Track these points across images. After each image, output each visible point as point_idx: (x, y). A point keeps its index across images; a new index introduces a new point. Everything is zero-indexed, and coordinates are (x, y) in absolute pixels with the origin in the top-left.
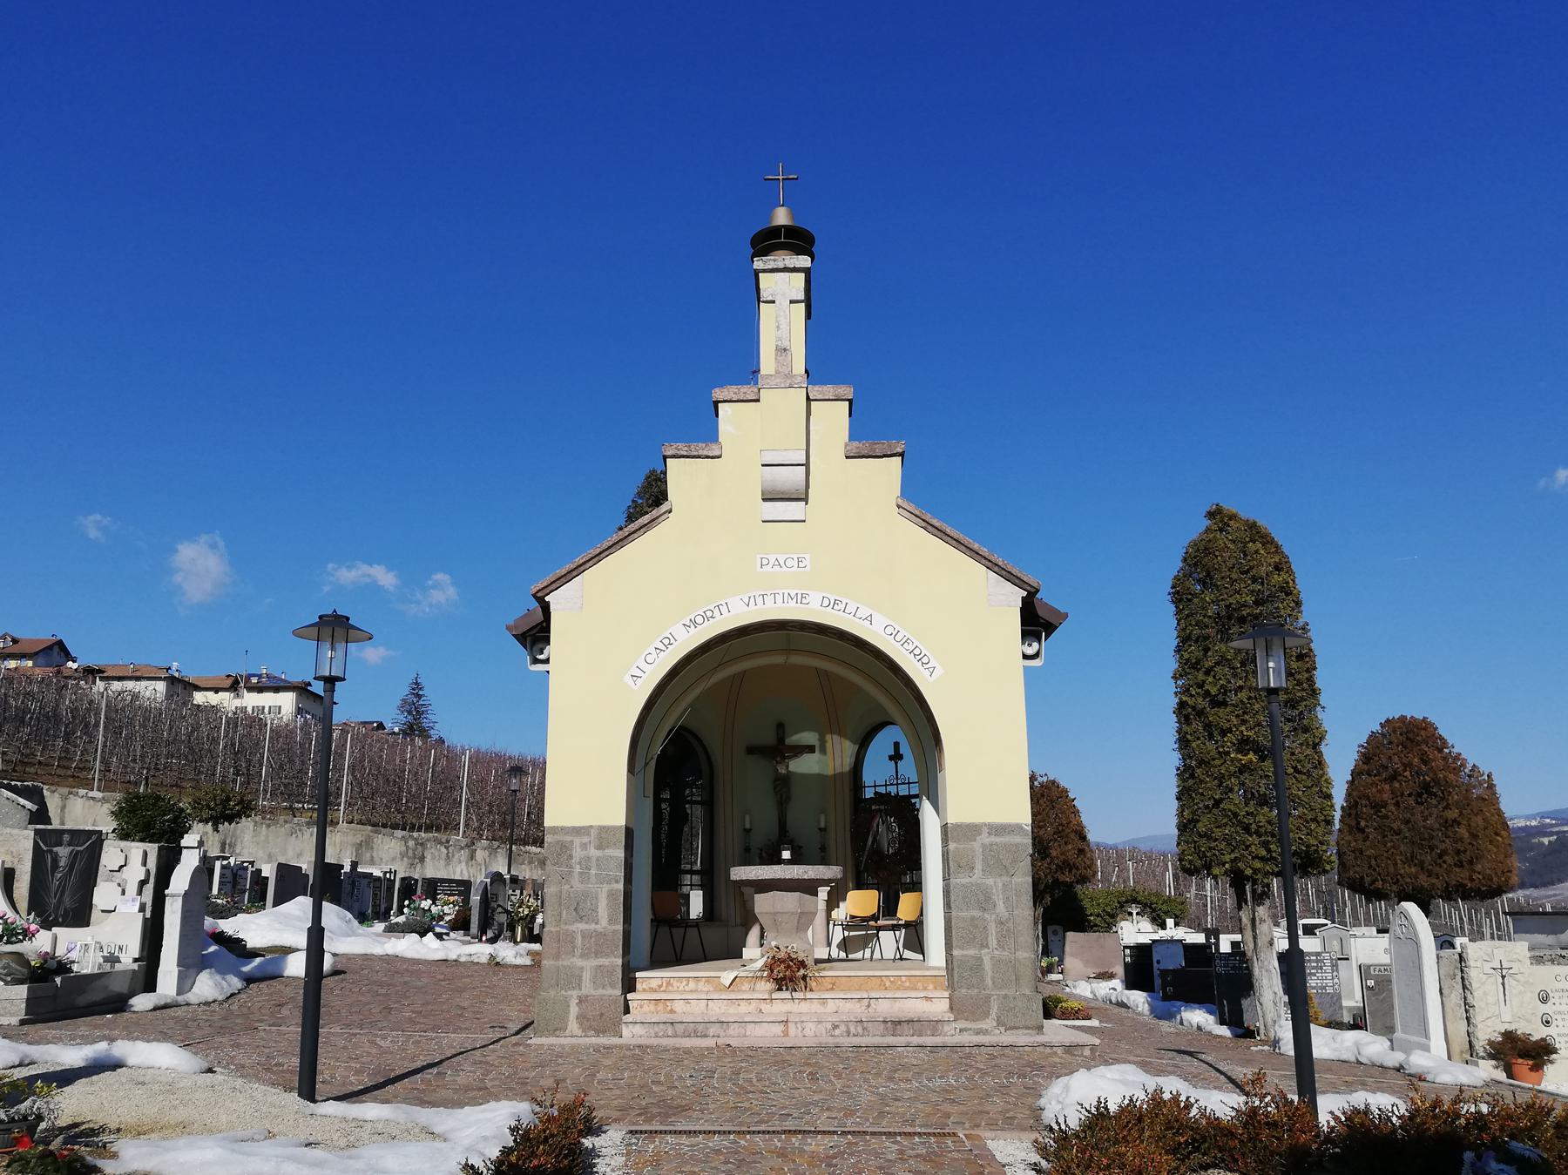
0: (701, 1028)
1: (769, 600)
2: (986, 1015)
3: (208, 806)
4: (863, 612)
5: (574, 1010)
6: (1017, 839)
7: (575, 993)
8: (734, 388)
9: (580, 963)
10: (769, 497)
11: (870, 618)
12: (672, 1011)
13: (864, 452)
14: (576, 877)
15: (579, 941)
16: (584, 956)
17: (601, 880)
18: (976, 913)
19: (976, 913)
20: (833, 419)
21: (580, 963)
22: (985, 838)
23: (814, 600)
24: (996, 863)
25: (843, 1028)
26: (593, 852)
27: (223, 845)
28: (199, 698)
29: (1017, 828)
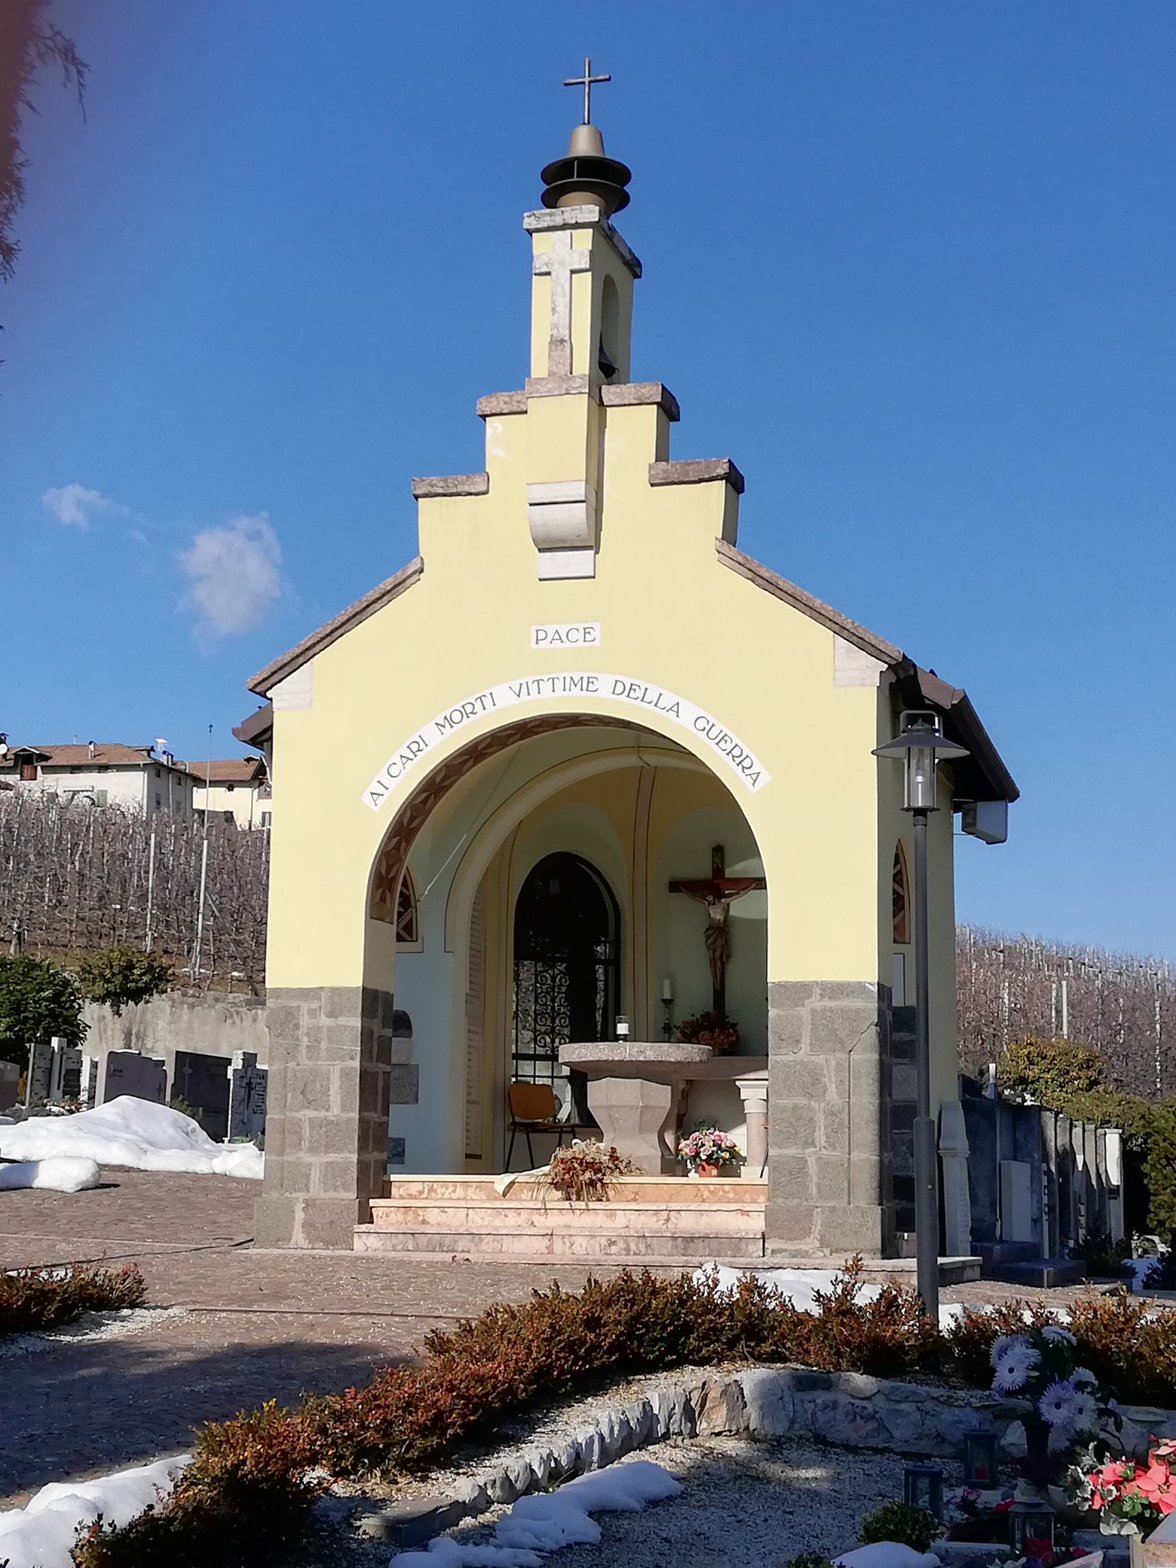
0: (447, 1240)
1: (546, 687)
2: (807, 1232)
3: (102, 975)
4: (668, 701)
5: (300, 1216)
6: (858, 1003)
7: (301, 1196)
8: (504, 396)
9: (307, 1158)
10: (547, 546)
11: (676, 709)
12: (424, 1222)
13: (675, 478)
14: (303, 1049)
15: (306, 1131)
16: (313, 1150)
17: (334, 1055)
18: (801, 1101)
19: (801, 1101)
20: (633, 428)
21: (307, 1158)
22: (815, 1002)
23: (605, 684)
24: (828, 1034)
25: (621, 1244)
26: (324, 1021)
27: (128, 1035)
28: (203, 799)
29: (857, 989)
